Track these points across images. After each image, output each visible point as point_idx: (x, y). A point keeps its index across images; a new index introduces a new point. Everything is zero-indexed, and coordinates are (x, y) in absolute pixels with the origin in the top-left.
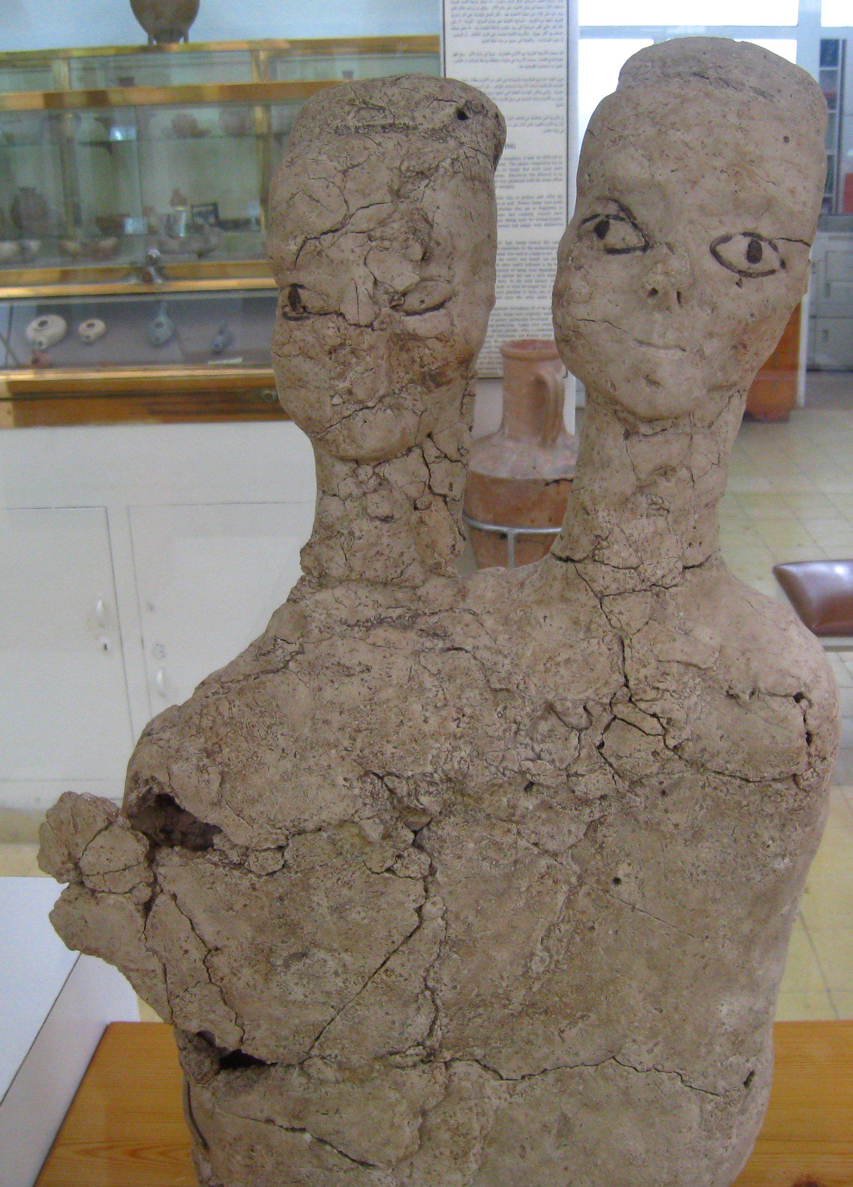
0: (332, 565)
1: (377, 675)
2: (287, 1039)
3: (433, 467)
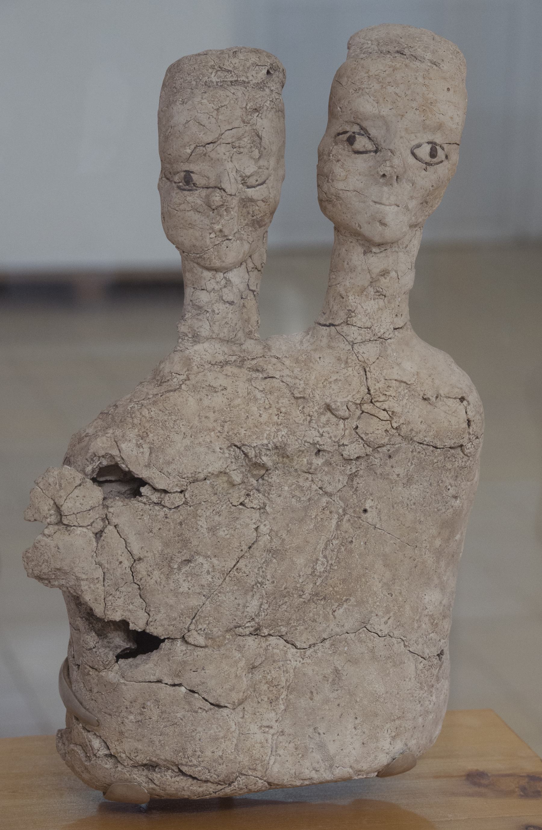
0: (202, 330)
1: (231, 392)
2: (175, 619)
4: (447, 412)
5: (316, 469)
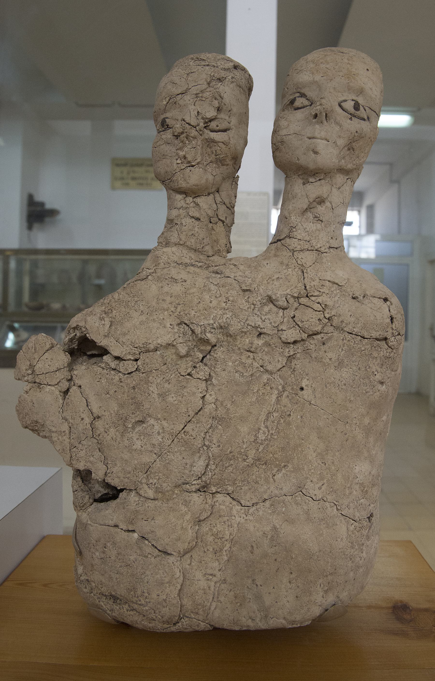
0: (172, 238)
1: (189, 284)
3: (219, 205)
4: (373, 308)
5: (256, 349)
